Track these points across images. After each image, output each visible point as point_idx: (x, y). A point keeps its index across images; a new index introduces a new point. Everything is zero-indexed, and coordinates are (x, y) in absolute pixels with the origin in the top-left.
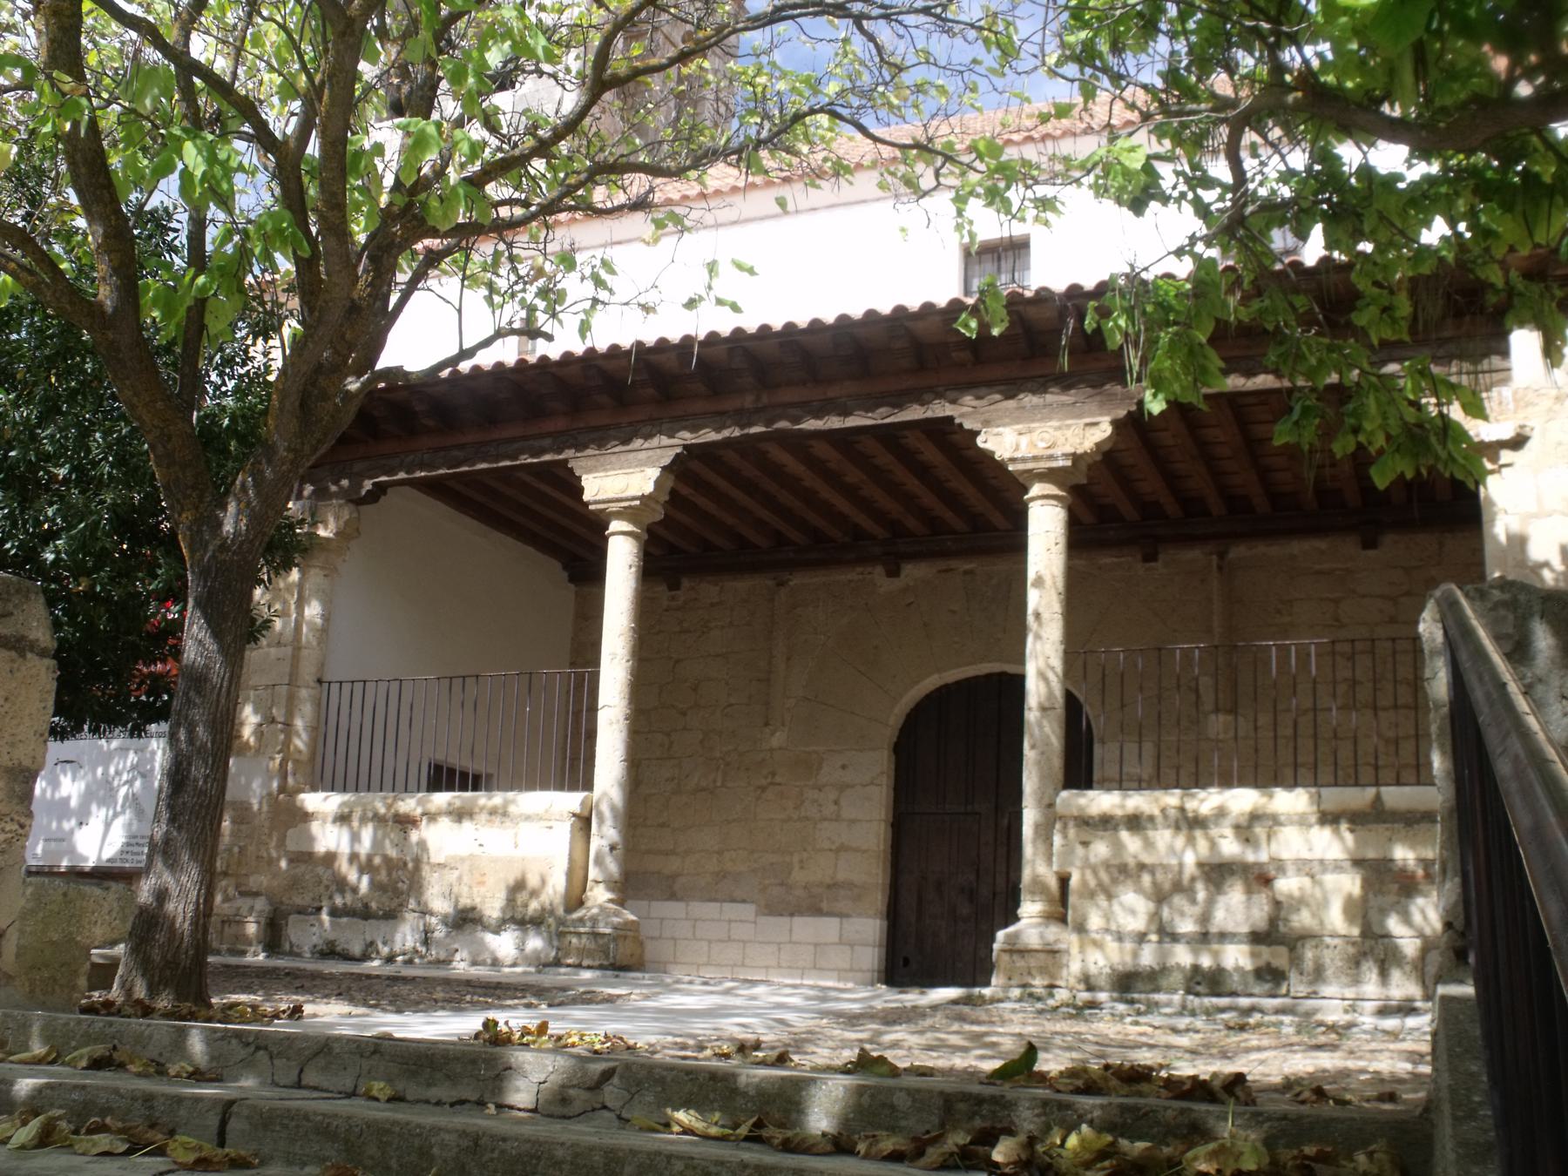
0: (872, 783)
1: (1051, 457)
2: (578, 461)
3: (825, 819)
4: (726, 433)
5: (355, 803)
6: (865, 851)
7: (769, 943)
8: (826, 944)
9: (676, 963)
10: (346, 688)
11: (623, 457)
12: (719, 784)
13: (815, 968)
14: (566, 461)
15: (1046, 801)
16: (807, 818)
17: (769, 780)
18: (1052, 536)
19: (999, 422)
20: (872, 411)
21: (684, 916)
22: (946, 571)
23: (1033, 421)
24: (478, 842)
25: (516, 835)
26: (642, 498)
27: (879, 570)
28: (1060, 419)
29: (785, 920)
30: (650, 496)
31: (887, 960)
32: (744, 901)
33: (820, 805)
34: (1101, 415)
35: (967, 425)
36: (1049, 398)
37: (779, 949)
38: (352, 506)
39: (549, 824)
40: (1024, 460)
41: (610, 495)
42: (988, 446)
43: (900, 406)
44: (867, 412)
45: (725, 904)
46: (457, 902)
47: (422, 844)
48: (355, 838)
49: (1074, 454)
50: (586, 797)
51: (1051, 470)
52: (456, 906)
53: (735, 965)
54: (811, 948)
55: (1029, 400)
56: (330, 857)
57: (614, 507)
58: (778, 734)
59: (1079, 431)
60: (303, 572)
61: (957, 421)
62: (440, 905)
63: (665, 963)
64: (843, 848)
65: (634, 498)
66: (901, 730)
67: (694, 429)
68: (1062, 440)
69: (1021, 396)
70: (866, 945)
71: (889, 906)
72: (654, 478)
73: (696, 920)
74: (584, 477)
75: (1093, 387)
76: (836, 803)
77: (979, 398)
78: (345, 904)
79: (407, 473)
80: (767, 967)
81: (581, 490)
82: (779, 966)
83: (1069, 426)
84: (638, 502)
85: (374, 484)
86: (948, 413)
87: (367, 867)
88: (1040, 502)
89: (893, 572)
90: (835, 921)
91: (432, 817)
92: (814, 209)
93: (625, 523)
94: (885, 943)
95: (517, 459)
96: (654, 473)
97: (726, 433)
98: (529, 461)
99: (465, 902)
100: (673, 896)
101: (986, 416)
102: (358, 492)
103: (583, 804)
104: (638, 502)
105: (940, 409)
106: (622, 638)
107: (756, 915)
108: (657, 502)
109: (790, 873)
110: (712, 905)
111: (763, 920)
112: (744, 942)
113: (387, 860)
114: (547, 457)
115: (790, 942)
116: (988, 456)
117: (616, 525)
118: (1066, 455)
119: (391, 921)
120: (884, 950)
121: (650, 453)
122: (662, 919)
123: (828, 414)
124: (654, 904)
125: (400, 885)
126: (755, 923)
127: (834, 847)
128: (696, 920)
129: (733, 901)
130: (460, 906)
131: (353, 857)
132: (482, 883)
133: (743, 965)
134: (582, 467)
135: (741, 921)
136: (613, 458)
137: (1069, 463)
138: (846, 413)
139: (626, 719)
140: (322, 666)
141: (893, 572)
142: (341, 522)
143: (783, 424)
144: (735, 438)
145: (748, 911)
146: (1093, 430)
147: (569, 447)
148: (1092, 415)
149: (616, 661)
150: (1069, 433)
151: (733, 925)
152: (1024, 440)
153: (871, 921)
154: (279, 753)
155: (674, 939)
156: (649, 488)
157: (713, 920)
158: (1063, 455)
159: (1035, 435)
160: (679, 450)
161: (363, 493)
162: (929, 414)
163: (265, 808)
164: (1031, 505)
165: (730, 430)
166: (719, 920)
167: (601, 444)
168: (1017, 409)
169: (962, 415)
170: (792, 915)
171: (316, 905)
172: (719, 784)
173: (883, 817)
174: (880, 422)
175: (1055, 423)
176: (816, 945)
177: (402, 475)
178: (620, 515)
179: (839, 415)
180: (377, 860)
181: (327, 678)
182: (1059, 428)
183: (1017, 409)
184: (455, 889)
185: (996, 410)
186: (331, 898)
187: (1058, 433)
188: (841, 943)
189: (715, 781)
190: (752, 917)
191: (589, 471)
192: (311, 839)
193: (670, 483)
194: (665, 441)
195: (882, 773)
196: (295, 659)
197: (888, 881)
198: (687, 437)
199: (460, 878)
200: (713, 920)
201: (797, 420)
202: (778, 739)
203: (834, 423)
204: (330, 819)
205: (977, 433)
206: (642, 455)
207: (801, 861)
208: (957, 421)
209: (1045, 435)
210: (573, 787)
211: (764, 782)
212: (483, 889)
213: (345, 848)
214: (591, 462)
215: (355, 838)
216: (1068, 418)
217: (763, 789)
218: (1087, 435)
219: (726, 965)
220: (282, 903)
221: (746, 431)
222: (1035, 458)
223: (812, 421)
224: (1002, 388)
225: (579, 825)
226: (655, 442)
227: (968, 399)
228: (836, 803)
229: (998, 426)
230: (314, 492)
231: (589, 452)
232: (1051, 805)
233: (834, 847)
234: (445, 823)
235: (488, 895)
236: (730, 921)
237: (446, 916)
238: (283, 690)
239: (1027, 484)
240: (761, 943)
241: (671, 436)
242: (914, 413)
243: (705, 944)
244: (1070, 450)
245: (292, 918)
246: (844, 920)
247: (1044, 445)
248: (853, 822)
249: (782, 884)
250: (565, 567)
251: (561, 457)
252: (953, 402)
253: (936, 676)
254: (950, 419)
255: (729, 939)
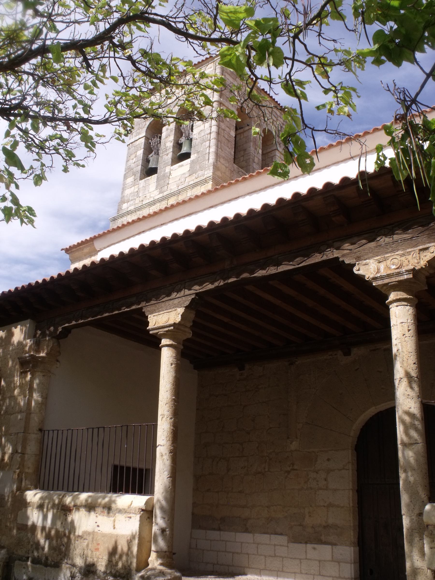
0: (344, 469)
1: (399, 274)
2: (147, 307)
3: (321, 489)
4: (216, 284)
5: (46, 497)
6: (343, 507)
7: (295, 558)
8: (325, 561)
9: (249, 568)
10: (56, 432)
11: (167, 303)
12: (267, 470)
13: (320, 575)
14: (142, 308)
15: (417, 512)
16: (311, 488)
17: (291, 468)
18: (406, 326)
19: (366, 257)
20: (292, 261)
21: (252, 542)
22: (374, 350)
23: (387, 253)
24: (97, 524)
25: (114, 521)
26: (174, 325)
27: (340, 352)
28: (404, 249)
29: (302, 546)
30: (180, 323)
31: (360, 571)
32: (281, 534)
33: (317, 481)
34: (430, 243)
35: (347, 262)
36: (396, 237)
37: (301, 563)
38: (54, 340)
39: (129, 516)
40: (382, 278)
41: (161, 324)
42: (361, 272)
43: (308, 256)
44: (290, 262)
45: (272, 536)
46: (86, 560)
47: (72, 522)
48: (45, 518)
49: (414, 270)
50: (149, 499)
51: (400, 282)
52: (86, 562)
53: (279, 571)
54: (317, 563)
55: (383, 240)
56: (34, 527)
57: (161, 331)
58: (294, 443)
59: (416, 255)
60: (32, 374)
61: (341, 259)
62: (79, 562)
63: (244, 567)
64: (331, 505)
65: (170, 326)
66: (359, 438)
67: (200, 284)
68: (406, 262)
69: (378, 239)
70: (347, 563)
71: (359, 538)
72: (181, 313)
73: (258, 544)
74: (149, 316)
75: (422, 226)
76: (326, 480)
77: (353, 244)
78: (38, 556)
79: (76, 321)
80: (295, 573)
81: (147, 323)
82: (301, 573)
83: (409, 253)
84: (172, 328)
85: (62, 328)
86: (335, 256)
87: (48, 537)
88: (395, 304)
89: (347, 353)
90: (329, 547)
91: (77, 507)
92: (297, 177)
93: (168, 340)
94: (358, 560)
95: (121, 310)
96: (181, 310)
97: (216, 284)
98: (126, 310)
99: (89, 560)
100: (246, 531)
101: (358, 254)
102: (56, 333)
103: (147, 503)
104: (172, 328)
105: (335, 254)
106: (167, 405)
107: (288, 542)
108: (186, 327)
109: (304, 519)
110: (266, 536)
111: (291, 545)
112: (283, 558)
113: (57, 532)
114: (134, 307)
115: (306, 559)
116: (361, 278)
117: (164, 341)
118: (408, 271)
119: (57, 569)
120: (358, 565)
121: (180, 299)
122: (242, 543)
123: (269, 266)
124: (238, 534)
125: (62, 547)
126: (288, 546)
127: (326, 505)
128: (258, 544)
129: (276, 534)
130: (87, 563)
131: (43, 528)
132: (97, 549)
133: (282, 571)
134: (149, 311)
135: (281, 545)
136: (163, 304)
137: (411, 276)
138: (278, 264)
139: (171, 452)
140: (42, 421)
141: (347, 353)
142: (49, 349)
143: (245, 275)
144: (222, 286)
145: (283, 540)
146: (423, 254)
147: (143, 301)
148: (424, 243)
149: (164, 419)
150: (410, 257)
151: (277, 547)
152: (382, 266)
153: (347, 548)
154: (18, 469)
155: (248, 554)
156: (178, 319)
157: (266, 544)
158: (406, 271)
159: (388, 262)
160: (193, 296)
161: (58, 333)
162: (325, 258)
163: (10, 500)
164: (390, 306)
165: (218, 282)
166: (269, 544)
167: (157, 298)
168: (376, 247)
169: (343, 256)
170: (306, 543)
171: (27, 555)
172: (267, 470)
173: (351, 487)
174: (297, 266)
175: (400, 252)
176: (320, 561)
177: (74, 323)
178: (166, 335)
179: (275, 266)
180: (53, 532)
181: (45, 428)
182: (403, 255)
183: (376, 247)
184: (86, 552)
185: (364, 250)
186: (33, 552)
187: (403, 258)
188: (332, 561)
189: (265, 468)
190: (286, 544)
191: (152, 313)
192: (27, 518)
193: (192, 316)
194: (187, 292)
195: (348, 463)
196: (27, 420)
197: (357, 523)
198: (197, 288)
199: (88, 545)
200: (266, 544)
201: (253, 272)
202: (294, 446)
203: (272, 270)
204: (36, 506)
205: (354, 265)
206: (176, 301)
207: (309, 513)
208: (341, 259)
209: (395, 261)
210: (140, 492)
211: (289, 469)
212: (98, 553)
213: (39, 524)
214: (153, 308)
215: (45, 518)
216: (408, 248)
217: (288, 472)
218: (422, 257)
219: (274, 571)
220: (13, 553)
221: (226, 282)
222: (389, 276)
223: (260, 271)
224: (366, 236)
225: (146, 516)
226: (182, 293)
227: (347, 246)
228: (326, 480)
229: (365, 260)
230: (41, 334)
231: (153, 302)
232: (420, 514)
233: (326, 505)
234: (83, 512)
235: (100, 557)
236: (275, 545)
237: (81, 568)
238: (21, 435)
239: (387, 293)
240: (291, 558)
241: (190, 289)
242: (316, 258)
243: (263, 557)
244: (411, 267)
245: (17, 562)
246: (334, 547)
247: (394, 267)
248: (335, 490)
249: (300, 525)
250: (191, 362)
251: (139, 306)
252: (338, 248)
253: (374, 408)
254: (337, 258)
255: (275, 556)
